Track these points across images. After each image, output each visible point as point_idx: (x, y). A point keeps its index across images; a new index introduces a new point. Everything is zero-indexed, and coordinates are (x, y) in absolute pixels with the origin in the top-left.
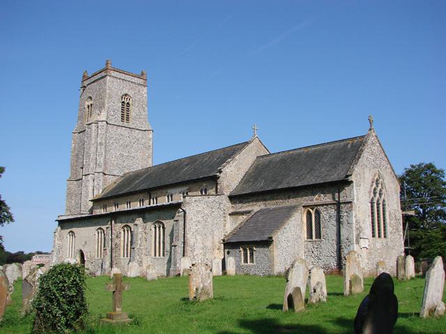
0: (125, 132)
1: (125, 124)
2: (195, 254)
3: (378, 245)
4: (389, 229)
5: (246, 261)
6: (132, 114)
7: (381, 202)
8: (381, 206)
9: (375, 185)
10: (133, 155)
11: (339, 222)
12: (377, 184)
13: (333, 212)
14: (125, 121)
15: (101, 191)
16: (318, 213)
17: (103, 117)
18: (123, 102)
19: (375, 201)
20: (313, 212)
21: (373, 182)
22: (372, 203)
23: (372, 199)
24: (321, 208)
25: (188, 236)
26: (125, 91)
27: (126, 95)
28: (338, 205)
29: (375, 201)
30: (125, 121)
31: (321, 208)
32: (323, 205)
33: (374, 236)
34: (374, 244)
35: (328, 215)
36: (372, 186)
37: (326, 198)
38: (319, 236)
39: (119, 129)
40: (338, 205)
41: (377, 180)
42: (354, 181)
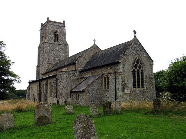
0: (56, 46)
1: (56, 43)
2: (62, 96)
3: (138, 92)
4: (145, 83)
5: (77, 100)
6: (59, 38)
7: (140, 71)
8: (140, 73)
9: (136, 63)
10: (60, 55)
11: (115, 82)
12: (138, 62)
13: (113, 77)
14: (56, 41)
15: (46, 70)
16: (108, 77)
17: (46, 41)
18: (55, 34)
19: (136, 70)
20: (106, 77)
21: (134, 62)
22: (134, 72)
23: (134, 70)
24: (109, 75)
25: (59, 89)
26: (56, 30)
27: (56, 31)
28: (115, 73)
29: (136, 70)
30: (56, 41)
31: (109, 75)
32: (109, 74)
33: (135, 87)
34: (135, 91)
35: (111, 77)
36: (134, 63)
37: (110, 70)
38: (108, 88)
39: (54, 45)
40: (115, 73)
41: (137, 61)
42: (121, 62)
